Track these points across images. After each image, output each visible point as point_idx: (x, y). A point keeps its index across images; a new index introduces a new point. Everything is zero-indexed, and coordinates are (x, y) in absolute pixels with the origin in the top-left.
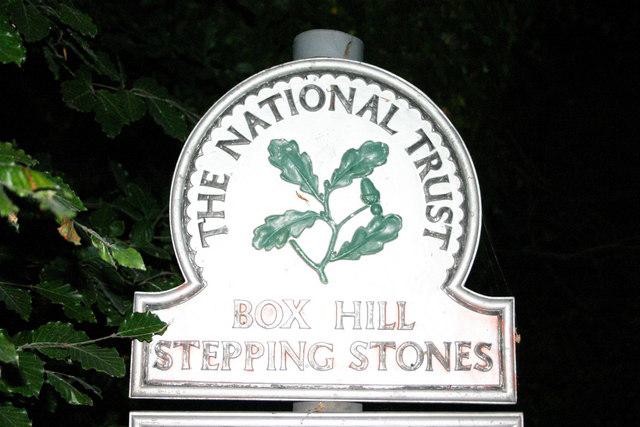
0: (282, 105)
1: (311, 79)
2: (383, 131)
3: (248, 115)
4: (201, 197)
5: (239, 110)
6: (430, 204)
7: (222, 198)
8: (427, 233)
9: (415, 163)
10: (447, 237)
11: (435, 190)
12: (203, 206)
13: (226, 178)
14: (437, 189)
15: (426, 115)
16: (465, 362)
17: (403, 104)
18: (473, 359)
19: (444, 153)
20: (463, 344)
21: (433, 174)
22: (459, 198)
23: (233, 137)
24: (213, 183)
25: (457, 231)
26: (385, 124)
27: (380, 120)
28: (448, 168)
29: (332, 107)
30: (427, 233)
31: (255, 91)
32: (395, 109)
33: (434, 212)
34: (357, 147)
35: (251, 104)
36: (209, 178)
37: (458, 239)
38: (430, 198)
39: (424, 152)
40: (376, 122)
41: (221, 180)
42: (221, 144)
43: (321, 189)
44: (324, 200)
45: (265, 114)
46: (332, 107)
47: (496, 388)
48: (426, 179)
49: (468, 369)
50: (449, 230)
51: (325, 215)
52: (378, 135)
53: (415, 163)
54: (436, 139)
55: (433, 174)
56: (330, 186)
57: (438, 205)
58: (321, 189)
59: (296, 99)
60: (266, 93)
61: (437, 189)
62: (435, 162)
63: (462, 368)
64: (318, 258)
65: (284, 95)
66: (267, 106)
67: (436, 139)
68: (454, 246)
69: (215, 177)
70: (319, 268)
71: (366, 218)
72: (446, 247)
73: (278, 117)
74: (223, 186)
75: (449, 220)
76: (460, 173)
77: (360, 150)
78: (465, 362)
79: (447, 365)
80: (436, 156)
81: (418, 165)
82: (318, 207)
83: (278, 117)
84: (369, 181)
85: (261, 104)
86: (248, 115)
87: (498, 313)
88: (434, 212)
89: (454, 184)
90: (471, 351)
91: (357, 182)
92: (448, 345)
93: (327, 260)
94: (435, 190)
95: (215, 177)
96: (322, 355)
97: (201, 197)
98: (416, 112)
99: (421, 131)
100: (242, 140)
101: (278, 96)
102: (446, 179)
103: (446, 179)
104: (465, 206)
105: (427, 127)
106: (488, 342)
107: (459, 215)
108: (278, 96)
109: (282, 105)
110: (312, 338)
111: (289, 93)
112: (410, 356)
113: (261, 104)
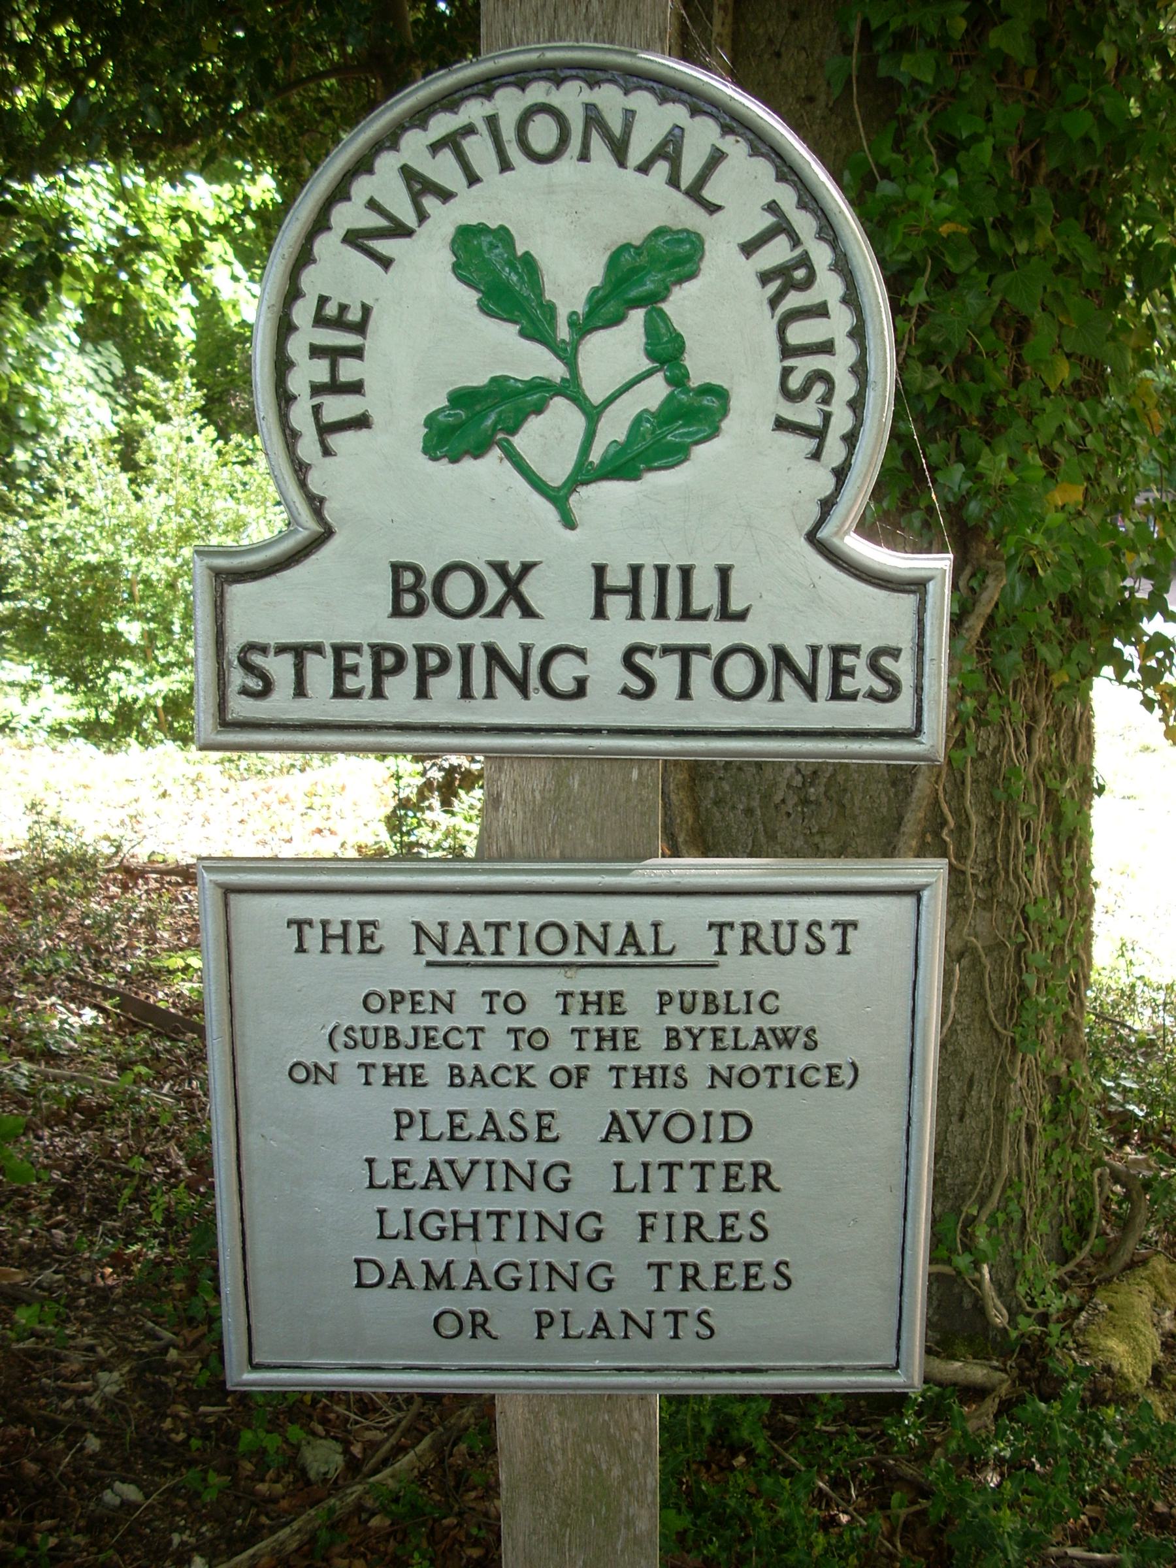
0: (479, 149)
1: (538, 92)
2: (688, 203)
3: (408, 174)
4: (316, 351)
5: (387, 163)
6: (790, 363)
7: (356, 353)
8: (782, 424)
9: (730, 567)
10: (819, 434)
11: (799, 333)
12: (320, 371)
13: (366, 310)
14: (801, 333)
15: (787, 171)
16: (847, 684)
17: (736, 148)
18: (864, 680)
19: (822, 256)
20: (837, 651)
21: (795, 299)
22: (847, 351)
23: (375, 221)
24: (338, 323)
25: (842, 420)
26: (694, 193)
27: (687, 179)
28: (829, 287)
29: (584, 157)
30: (782, 424)
31: (420, 117)
32: (717, 158)
33: (795, 383)
34: (676, 290)
35: (414, 145)
36: (331, 310)
37: (329, 228)
38: (787, 351)
39: (778, 252)
40: (678, 187)
41: (354, 315)
42: (354, 238)
43: (564, 332)
44: (568, 355)
45: (444, 169)
46: (584, 157)
47: (913, 734)
48: (490, 1283)
49: (852, 697)
50: (827, 417)
51: (571, 390)
52: (691, 217)
53: (730, 567)
54: (804, 223)
55: (795, 299)
56: (584, 326)
57: (805, 365)
58: (564, 332)
59: (508, 133)
60: (442, 124)
61: (801, 333)
62: (800, 274)
63: (837, 694)
64: (557, 473)
65: (482, 127)
66: (447, 155)
67: (804, 223)
68: (835, 451)
69: (343, 308)
70: (558, 498)
71: (655, 392)
72: (816, 455)
73: (473, 179)
74: (360, 328)
75: (826, 400)
76: (851, 299)
77: (668, 290)
78: (847, 684)
79: (810, 690)
80: (804, 261)
81: (765, 278)
82: (556, 370)
83: (473, 179)
84: (661, 313)
85: (435, 148)
86: (408, 174)
87: (917, 586)
88: (795, 383)
89: (841, 320)
90: (860, 664)
91: (637, 316)
92: (815, 651)
93: (584, 475)
94: (799, 333)
95: (343, 308)
96: (563, 673)
97: (316, 351)
98: (764, 168)
99: (772, 207)
100: (400, 230)
101: (469, 130)
102: (821, 311)
103: (821, 311)
104: (860, 370)
105: (787, 197)
106: (892, 643)
107: (846, 387)
108: (469, 130)
109: (479, 149)
110: (542, 639)
111: (492, 121)
112: (739, 674)
113: (435, 148)
